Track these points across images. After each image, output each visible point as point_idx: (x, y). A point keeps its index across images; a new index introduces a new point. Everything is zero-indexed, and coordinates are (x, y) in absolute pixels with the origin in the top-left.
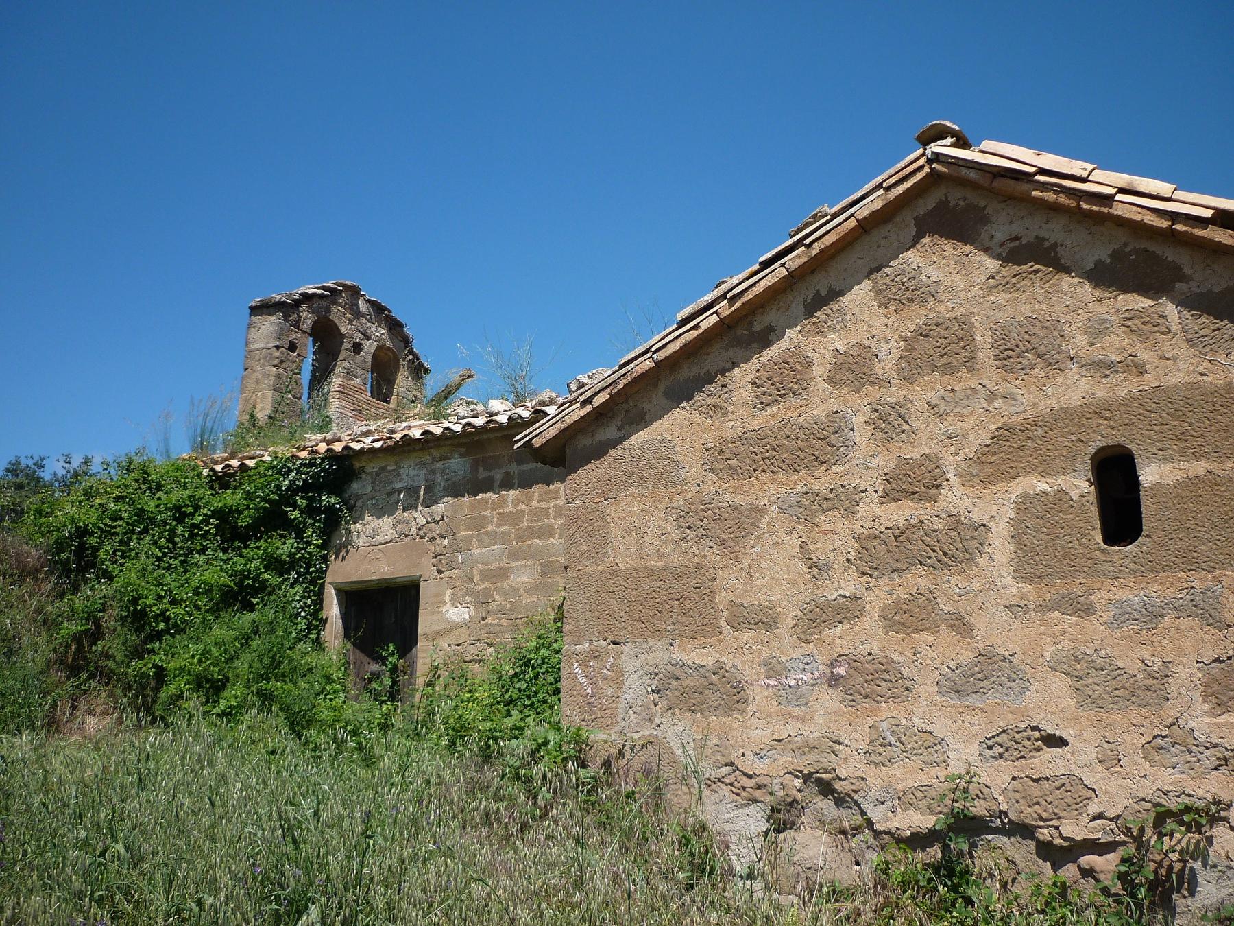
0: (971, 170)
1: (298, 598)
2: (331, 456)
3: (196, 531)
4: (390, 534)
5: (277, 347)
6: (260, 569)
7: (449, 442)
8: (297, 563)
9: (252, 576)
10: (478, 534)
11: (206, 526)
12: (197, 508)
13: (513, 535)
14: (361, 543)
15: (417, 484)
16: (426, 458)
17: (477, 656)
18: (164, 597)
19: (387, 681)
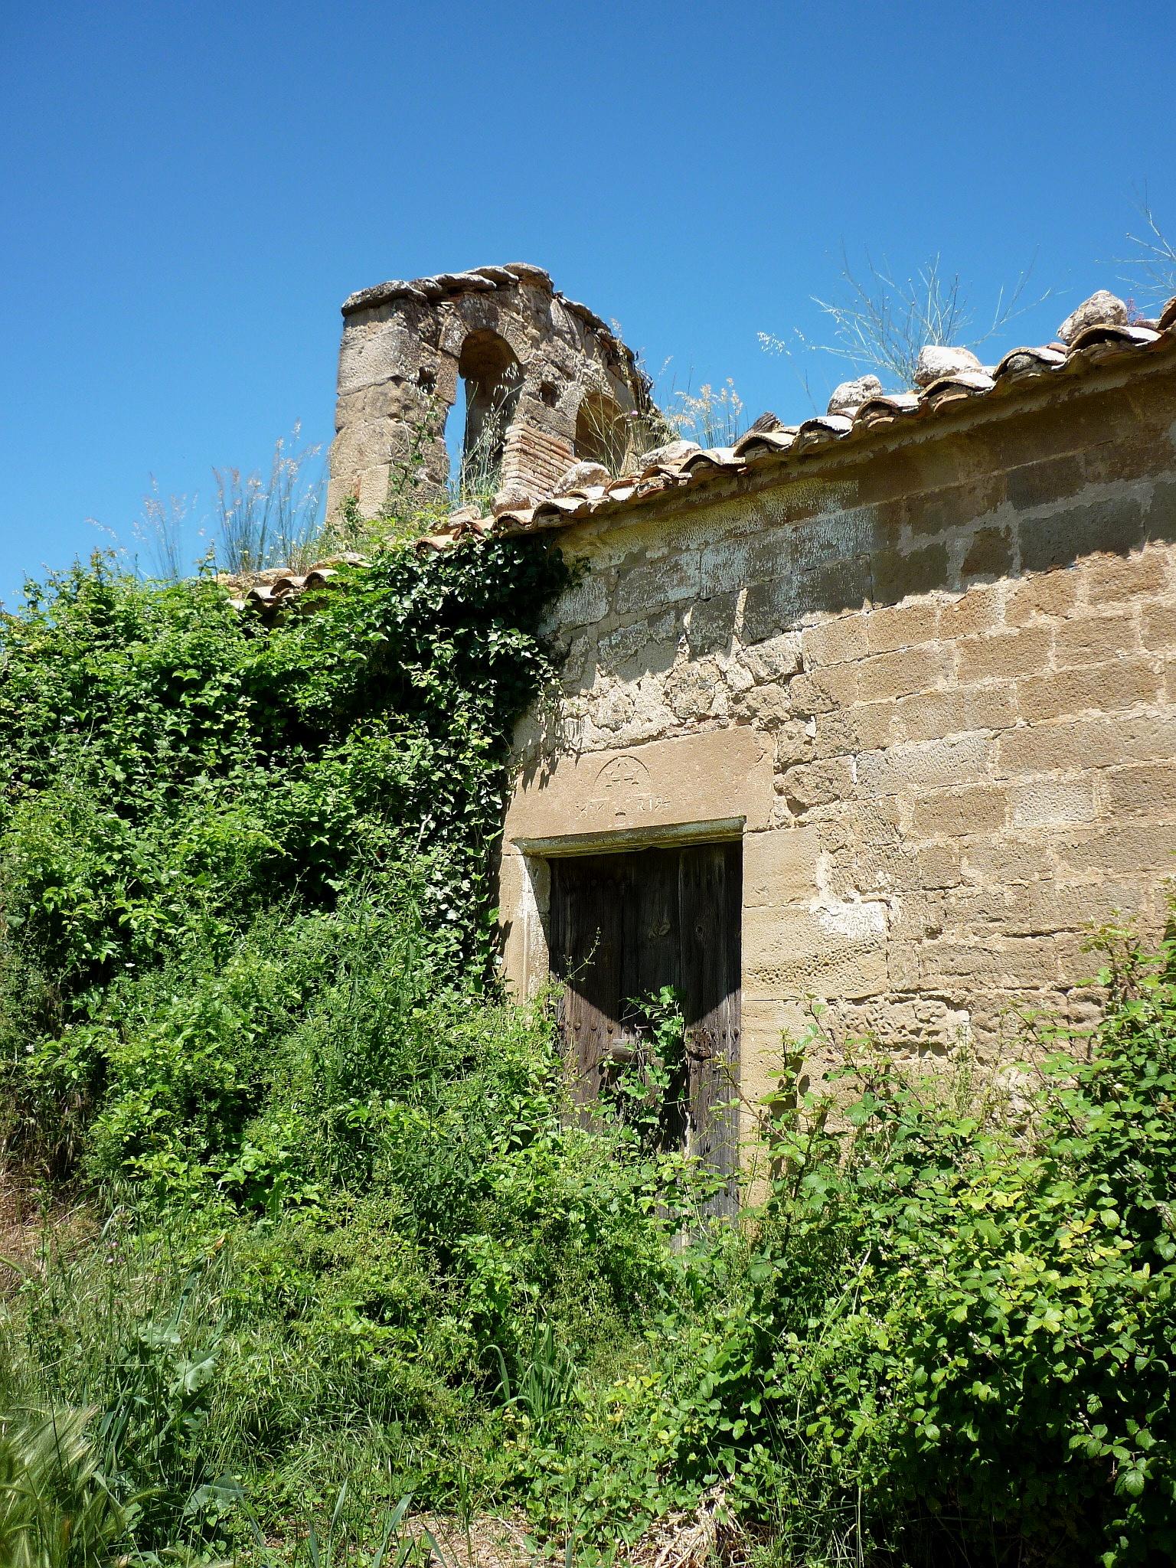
0: (646, 735)
1: (438, 876)
2: (509, 535)
3: (207, 724)
4: (661, 717)
5: (397, 380)
6: (346, 808)
7: (813, 467)
8: (435, 793)
9: (328, 825)
10: (908, 703)
11: (229, 711)
12: (208, 672)
13: (1013, 701)
14: (587, 743)
15: (726, 585)
16: (748, 520)
17: (916, 1032)
18: (114, 878)
19: (658, 1078)
